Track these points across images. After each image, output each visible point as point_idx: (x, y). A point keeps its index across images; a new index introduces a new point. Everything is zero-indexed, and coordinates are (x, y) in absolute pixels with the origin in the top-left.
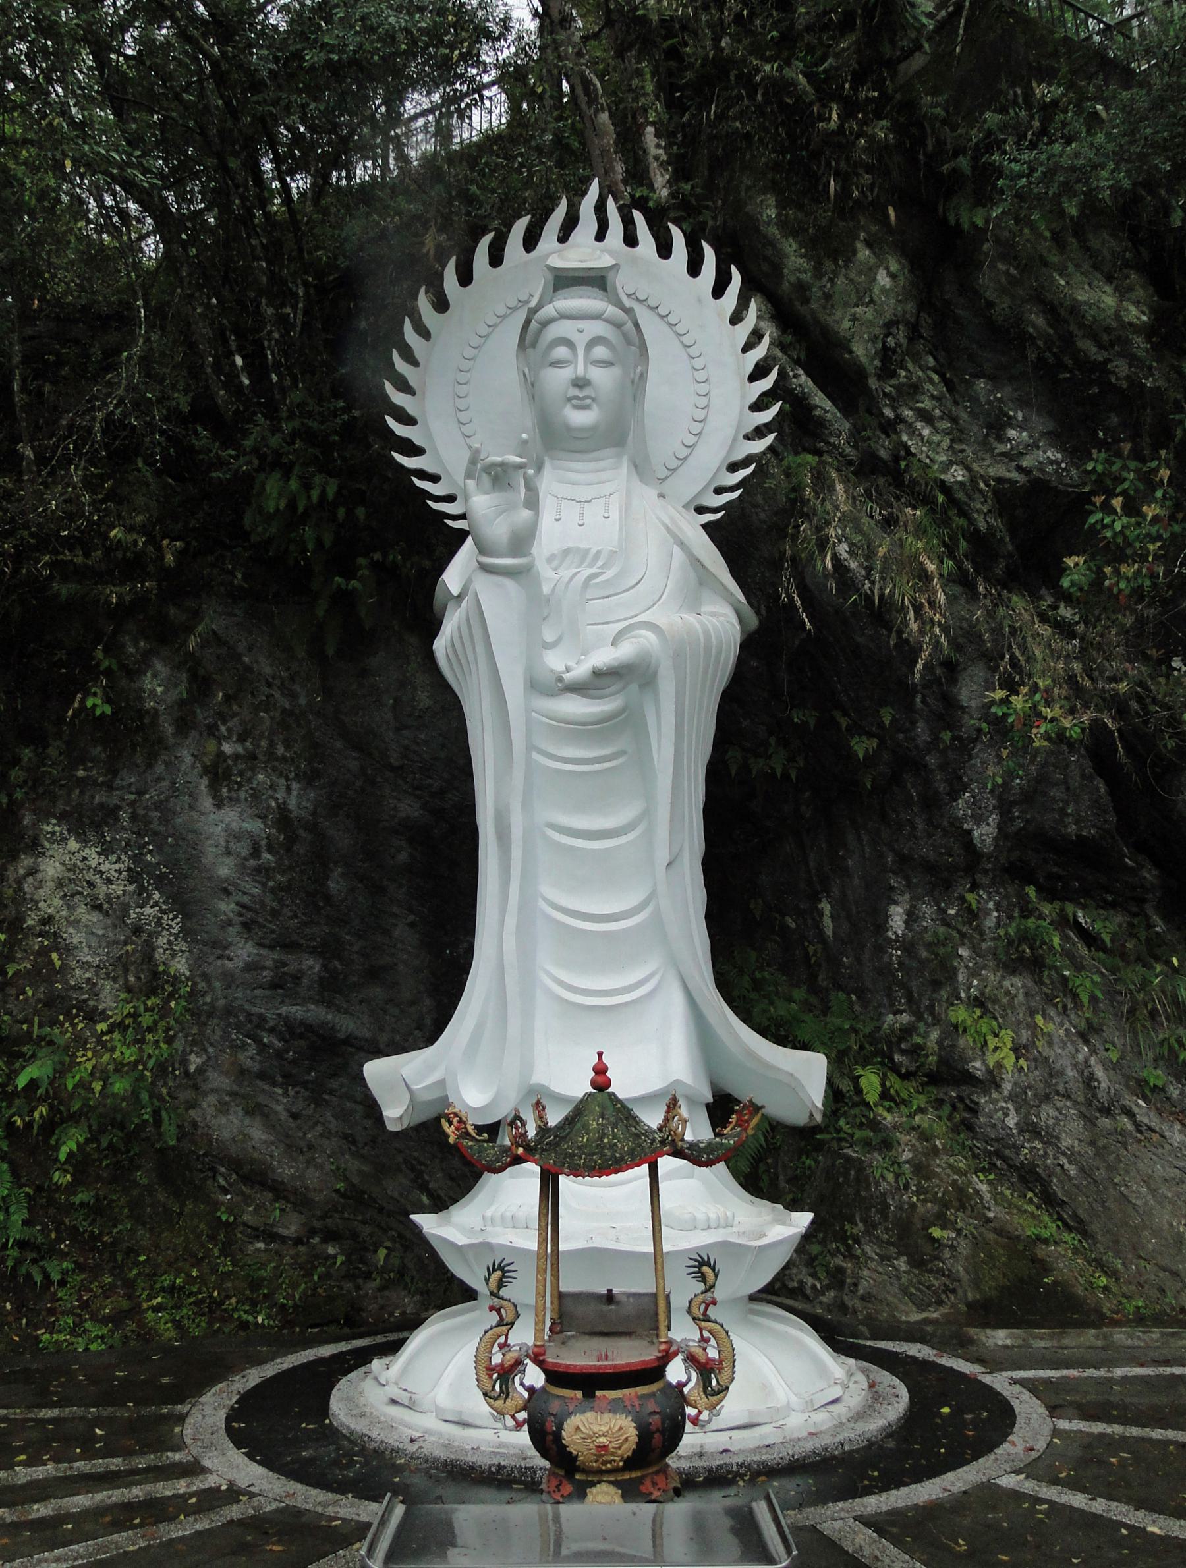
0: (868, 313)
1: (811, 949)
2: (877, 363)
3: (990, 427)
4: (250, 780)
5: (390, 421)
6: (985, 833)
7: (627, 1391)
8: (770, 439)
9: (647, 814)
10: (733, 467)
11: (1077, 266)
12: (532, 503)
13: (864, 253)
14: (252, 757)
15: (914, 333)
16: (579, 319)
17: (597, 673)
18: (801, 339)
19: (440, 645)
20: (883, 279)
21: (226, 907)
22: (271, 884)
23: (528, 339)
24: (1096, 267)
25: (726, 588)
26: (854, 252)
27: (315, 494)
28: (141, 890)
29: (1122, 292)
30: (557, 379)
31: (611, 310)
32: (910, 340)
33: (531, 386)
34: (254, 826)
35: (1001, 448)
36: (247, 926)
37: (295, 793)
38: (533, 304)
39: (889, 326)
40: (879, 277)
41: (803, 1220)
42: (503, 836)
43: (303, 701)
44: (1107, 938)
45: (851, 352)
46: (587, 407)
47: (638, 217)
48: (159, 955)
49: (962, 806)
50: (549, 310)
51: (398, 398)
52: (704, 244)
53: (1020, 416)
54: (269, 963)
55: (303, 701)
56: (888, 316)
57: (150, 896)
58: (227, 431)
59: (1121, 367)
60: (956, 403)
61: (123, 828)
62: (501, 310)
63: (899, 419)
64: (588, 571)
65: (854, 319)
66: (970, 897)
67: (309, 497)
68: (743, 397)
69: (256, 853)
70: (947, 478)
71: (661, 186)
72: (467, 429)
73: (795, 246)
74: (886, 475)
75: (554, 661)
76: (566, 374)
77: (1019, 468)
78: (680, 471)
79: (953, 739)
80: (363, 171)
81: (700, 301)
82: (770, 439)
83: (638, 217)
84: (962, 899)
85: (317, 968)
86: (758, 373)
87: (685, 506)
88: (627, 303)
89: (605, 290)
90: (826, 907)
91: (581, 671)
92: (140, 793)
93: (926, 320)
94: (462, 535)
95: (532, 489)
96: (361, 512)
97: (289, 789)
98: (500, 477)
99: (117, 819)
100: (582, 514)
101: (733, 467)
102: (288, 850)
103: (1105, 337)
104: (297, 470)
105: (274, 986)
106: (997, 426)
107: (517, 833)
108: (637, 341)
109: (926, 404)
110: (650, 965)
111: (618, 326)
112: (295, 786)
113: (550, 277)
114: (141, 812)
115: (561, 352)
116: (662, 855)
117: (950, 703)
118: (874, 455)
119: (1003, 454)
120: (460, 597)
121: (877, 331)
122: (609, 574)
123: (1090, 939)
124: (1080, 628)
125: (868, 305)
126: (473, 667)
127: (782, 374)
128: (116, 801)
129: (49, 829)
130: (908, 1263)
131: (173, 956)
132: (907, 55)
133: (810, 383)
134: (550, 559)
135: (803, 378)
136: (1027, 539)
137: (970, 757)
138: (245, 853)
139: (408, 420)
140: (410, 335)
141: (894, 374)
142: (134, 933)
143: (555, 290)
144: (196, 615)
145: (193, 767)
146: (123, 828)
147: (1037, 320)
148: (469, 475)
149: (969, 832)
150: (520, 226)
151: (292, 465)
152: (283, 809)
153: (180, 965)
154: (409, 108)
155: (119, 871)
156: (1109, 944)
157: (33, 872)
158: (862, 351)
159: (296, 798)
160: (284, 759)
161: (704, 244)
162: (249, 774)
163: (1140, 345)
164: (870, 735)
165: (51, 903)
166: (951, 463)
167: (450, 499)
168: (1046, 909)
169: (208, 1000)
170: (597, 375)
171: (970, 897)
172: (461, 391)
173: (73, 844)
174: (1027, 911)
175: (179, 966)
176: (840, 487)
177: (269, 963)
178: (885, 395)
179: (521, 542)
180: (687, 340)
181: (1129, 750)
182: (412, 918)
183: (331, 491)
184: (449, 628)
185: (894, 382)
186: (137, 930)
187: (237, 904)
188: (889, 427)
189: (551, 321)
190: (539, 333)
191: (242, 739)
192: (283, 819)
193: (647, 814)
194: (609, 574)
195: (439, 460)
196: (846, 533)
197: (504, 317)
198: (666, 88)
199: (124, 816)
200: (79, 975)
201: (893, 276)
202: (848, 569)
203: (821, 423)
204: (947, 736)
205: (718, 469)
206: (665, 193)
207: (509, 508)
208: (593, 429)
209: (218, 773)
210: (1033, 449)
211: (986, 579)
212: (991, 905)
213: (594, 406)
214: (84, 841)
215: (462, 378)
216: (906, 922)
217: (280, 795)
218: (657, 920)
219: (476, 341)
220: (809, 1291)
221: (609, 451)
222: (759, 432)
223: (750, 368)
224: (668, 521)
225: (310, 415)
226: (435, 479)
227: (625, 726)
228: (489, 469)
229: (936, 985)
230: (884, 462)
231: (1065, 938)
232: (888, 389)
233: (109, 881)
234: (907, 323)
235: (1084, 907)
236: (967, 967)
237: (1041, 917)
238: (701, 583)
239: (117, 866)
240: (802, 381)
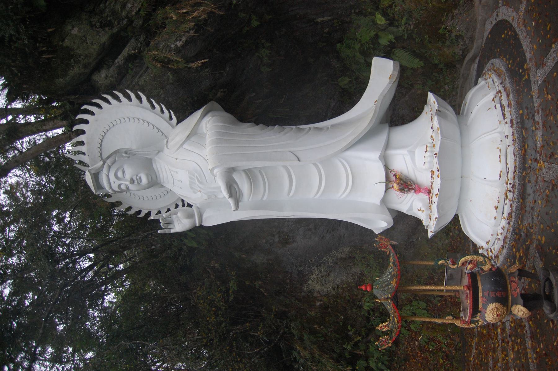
0: (89, 37)
2: (107, 29)
7: (480, 301)
10: (153, 107)
17: (231, 196)
20: (75, 31)
21: (328, 237)
26: (67, 47)
31: (106, 166)
39: (92, 26)
40: (75, 33)
41: (431, 97)
45: (105, 43)
46: (140, 178)
48: (343, 256)
52: (77, 118)
56: (89, 27)
61: (304, 269)
63: (127, 17)
64: (197, 183)
65: (92, 44)
69: (310, 230)
73: (71, 71)
90: (319, 20)
101: (153, 107)
109: (118, 7)
111: (109, 167)
114: (299, 264)
121: (95, 32)
129: (305, 289)
130: (455, 10)
131: (344, 252)
133: (120, 57)
141: (110, 21)
146: (304, 269)
153: (347, 250)
155: (318, 269)
157: (319, 292)
158: (104, 38)
161: (77, 118)
165: (328, 288)
170: (128, 176)
173: (310, 282)
178: (119, 24)
189: (113, 190)
191: (274, 236)
199: (300, 269)
200: (350, 279)
205: (155, 113)
208: (147, 175)
213: (139, 175)
214: (309, 279)
220: (464, 47)
221: (154, 164)
232: (116, 23)
233: (321, 272)
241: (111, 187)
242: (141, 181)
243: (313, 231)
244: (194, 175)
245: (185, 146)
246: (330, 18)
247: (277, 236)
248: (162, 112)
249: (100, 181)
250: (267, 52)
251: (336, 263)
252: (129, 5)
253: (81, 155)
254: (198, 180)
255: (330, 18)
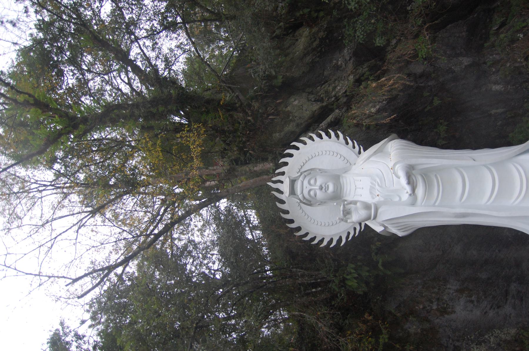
1: (509, 116)
2: (319, 103)
3: (338, 69)
4: (446, 301)
5: (332, 246)
6: (466, 61)
8: (339, 132)
9: (457, 168)
10: (347, 143)
11: (293, 49)
12: (355, 203)
13: (289, 108)
14: (438, 299)
15: (311, 93)
16: (304, 187)
17: (409, 183)
18: (314, 125)
19: (400, 234)
20: (296, 103)
21: (491, 314)
22: (483, 297)
23: (309, 203)
24: (294, 44)
25: (383, 144)
26: (288, 111)
27: (353, 271)
28: (484, 342)
29: (301, 35)
30: (320, 195)
31: (301, 178)
32: (313, 94)
33: (322, 203)
34: (462, 301)
35: (344, 66)
36: (499, 307)
37: (451, 287)
38: (299, 201)
42: (464, 215)
43: (419, 281)
44: (502, 19)
46: (328, 186)
47: (277, 171)
48: (508, 338)
49: (457, 69)
50: (300, 196)
51: (325, 243)
53: (335, 61)
54: (513, 301)
55: (419, 281)
57: (486, 339)
58: (334, 297)
59: (321, 34)
60: (331, 80)
62: (301, 211)
63: (335, 96)
64: (377, 186)
65: (306, 110)
66: (488, 64)
67: (354, 273)
68: (327, 141)
69: (472, 302)
70: (352, 80)
71: (269, 165)
72: (334, 223)
73: (286, 128)
74: (350, 100)
75: (405, 197)
76: (318, 192)
77: (349, 60)
78: (345, 156)
79: (434, 73)
80: (265, 250)
81: (300, 154)
82: (339, 132)
83: (277, 171)
84: (489, 67)
85: (515, 285)
86: (320, 137)
87: (358, 157)
88: (300, 174)
89: (295, 180)
90: (493, 112)
91: (408, 189)
92: (449, 338)
93: (309, 90)
94: (366, 225)
95: (351, 203)
96: (359, 257)
97: (449, 289)
98: (347, 213)
99: (458, 346)
100: (360, 188)
101: (347, 143)
102: (471, 290)
103: (313, 39)
104: (345, 276)
105: (522, 300)
106: (337, 68)
107: (462, 211)
108: (310, 171)
109: (331, 88)
110: (511, 167)
111: (305, 176)
112: (448, 286)
113: (292, 196)
115: (312, 193)
116: (471, 163)
117: (422, 76)
118: (345, 103)
119: (345, 66)
120: (385, 227)
122: (378, 180)
123: (503, 25)
124: (398, 38)
125: (303, 107)
126: (406, 223)
127: (322, 130)
128: (452, 346)
131: (509, 334)
132: (240, 100)
134: (373, 198)
135: (323, 124)
136: (372, 58)
137: (440, 67)
138: (472, 305)
139: (331, 241)
140: (307, 238)
141: (322, 98)
142: (500, 346)
143: (295, 195)
144: (390, 312)
145: (441, 319)
147: (308, 59)
148: (346, 221)
149: (466, 66)
150: (279, 205)
151: (343, 277)
152: (457, 291)
153: (513, 331)
154: (250, 237)
156: (504, 18)
158: (316, 107)
159: (453, 286)
160: (439, 289)
162: (444, 301)
163: (314, 30)
164: (433, 99)
166: (348, 80)
167: (355, 229)
168: (492, 39)
169: (526, 323)
170: (318, 183)
171: (488, 64)
172: (324, 225)
174: (493, 46)
175: (513, 332)
176: (353, 112)
177: (513, 301)
178: (328, 100)
179: (367, 207)
180: (310, 157)
181: (437, 19)
182: (497, 251)
183: (353, 266)
184: (394, 230)
185: (324, 98)
186: (499, 345)
187: (490, 309)
188: (337, 99)
190: (307, 200)
191: (432, 302)
192: (460, 291)
193: (457, 168)
194: (378, 180)
195: (343, 232)
196: (368, 109)
197: (301, 208)
198: (246, 163)
199: (457, 344)
201: (295, 100)
202: (379, 109)
203: (336, 119)
204: (433, 75)
206: (271, 164)
207: (356, 209)
208: (334, 184)
209: (443, 311)
210: (344, 57)
211: (383, 67)
212: (491, 57)
215: (319, 224)
216: (498, 84)
217: (451, 292)
218: (495, 164)
219: (306, 217)
221: (341, 180)
222: (337, 136)
223: (319, 139)
224: (362, 162)
225: (330, 270)
226: (349, 233)
227: (426, 175)
228: (345, 215)
229: (520, 73)
230: (347, 100)
231: (502, 33)
232: (326, 99)
234: (308, 95)
235: (491, 28)
236: (513, 63)
237: (495, 41)
238: (382, 151)
239: (475, 349)
240: (324, 124)
241: (302, 192)
242: (328, 189)
243: (475, 303)
244: (375, 181)
245: (371, 159)
246: (503, 110)
247: (435, 303)
248: (354, 147)
249: (295, 187)
250: (445, 128)
251: (499, 345)
252: (339, 88)
253: (279, 184)
254: (378, 185)
255: (503, 110)
